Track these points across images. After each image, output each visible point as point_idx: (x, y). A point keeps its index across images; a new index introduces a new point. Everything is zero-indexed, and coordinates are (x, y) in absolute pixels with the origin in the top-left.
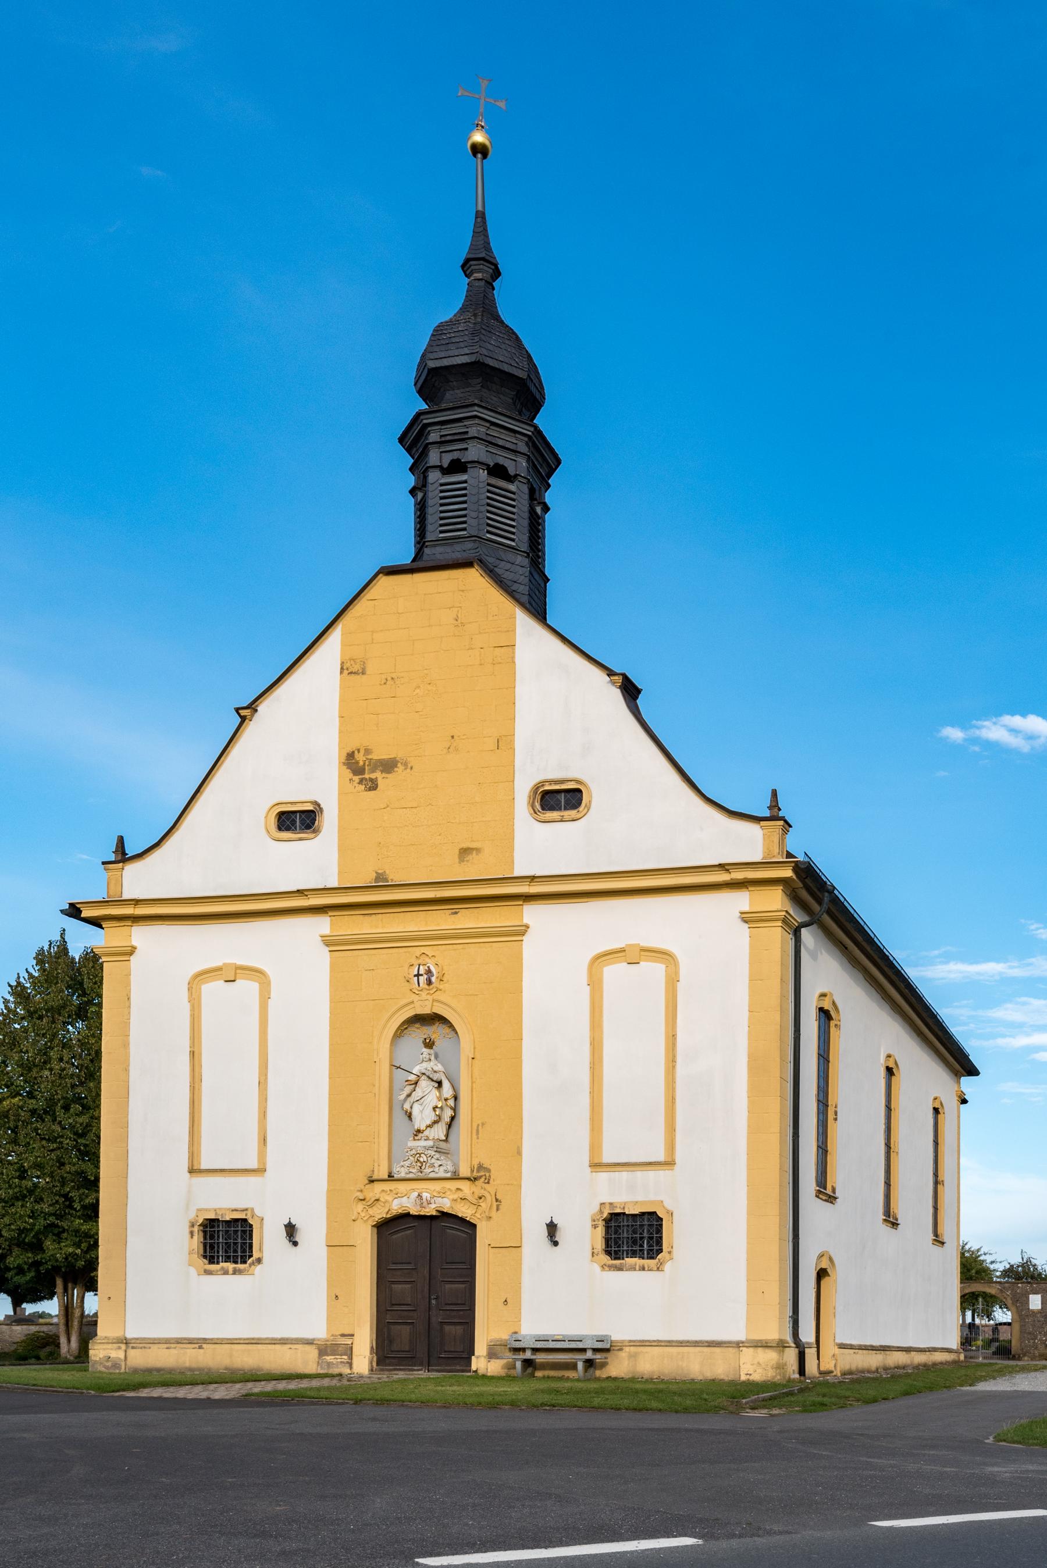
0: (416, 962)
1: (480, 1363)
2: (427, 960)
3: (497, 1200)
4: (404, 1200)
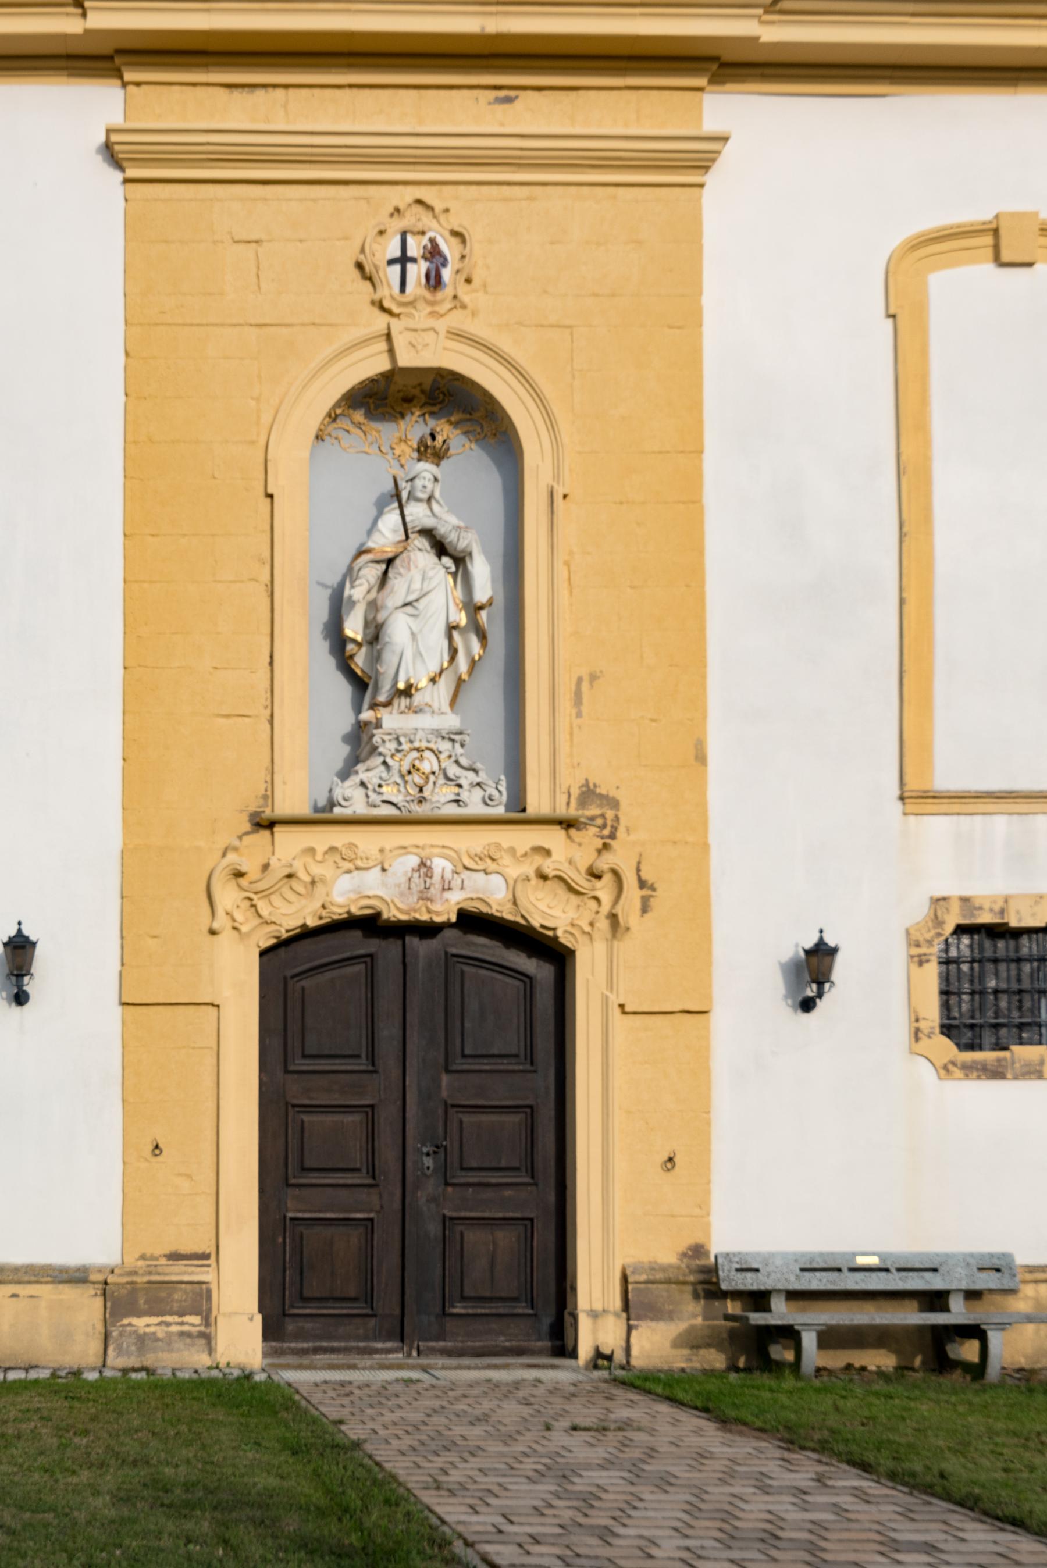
0: (396, 225)
1: (597, 1329)
2: (426, 220)
4: (377, 877)
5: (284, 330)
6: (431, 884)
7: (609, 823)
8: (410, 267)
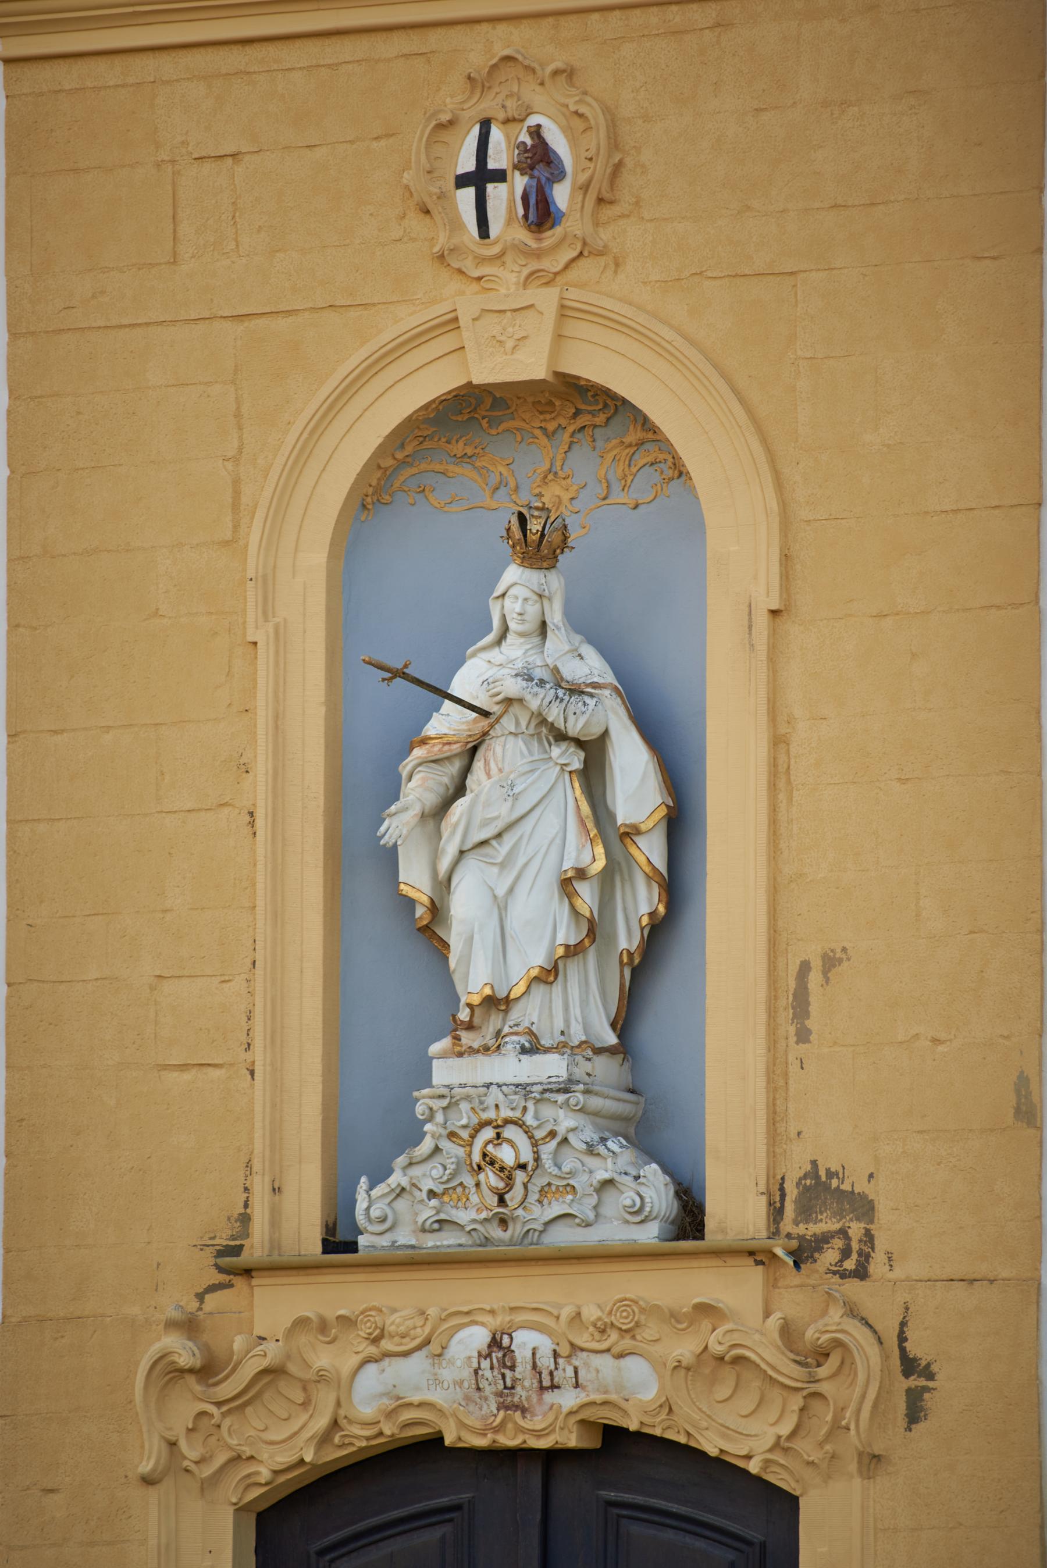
3: (909, 1365)
5: (282, 324)
6: (515, 1380)
7: (855, 1246)
8: (495, 192)
